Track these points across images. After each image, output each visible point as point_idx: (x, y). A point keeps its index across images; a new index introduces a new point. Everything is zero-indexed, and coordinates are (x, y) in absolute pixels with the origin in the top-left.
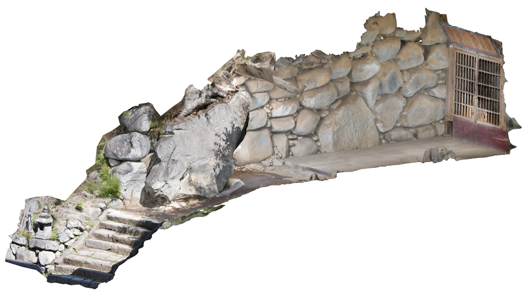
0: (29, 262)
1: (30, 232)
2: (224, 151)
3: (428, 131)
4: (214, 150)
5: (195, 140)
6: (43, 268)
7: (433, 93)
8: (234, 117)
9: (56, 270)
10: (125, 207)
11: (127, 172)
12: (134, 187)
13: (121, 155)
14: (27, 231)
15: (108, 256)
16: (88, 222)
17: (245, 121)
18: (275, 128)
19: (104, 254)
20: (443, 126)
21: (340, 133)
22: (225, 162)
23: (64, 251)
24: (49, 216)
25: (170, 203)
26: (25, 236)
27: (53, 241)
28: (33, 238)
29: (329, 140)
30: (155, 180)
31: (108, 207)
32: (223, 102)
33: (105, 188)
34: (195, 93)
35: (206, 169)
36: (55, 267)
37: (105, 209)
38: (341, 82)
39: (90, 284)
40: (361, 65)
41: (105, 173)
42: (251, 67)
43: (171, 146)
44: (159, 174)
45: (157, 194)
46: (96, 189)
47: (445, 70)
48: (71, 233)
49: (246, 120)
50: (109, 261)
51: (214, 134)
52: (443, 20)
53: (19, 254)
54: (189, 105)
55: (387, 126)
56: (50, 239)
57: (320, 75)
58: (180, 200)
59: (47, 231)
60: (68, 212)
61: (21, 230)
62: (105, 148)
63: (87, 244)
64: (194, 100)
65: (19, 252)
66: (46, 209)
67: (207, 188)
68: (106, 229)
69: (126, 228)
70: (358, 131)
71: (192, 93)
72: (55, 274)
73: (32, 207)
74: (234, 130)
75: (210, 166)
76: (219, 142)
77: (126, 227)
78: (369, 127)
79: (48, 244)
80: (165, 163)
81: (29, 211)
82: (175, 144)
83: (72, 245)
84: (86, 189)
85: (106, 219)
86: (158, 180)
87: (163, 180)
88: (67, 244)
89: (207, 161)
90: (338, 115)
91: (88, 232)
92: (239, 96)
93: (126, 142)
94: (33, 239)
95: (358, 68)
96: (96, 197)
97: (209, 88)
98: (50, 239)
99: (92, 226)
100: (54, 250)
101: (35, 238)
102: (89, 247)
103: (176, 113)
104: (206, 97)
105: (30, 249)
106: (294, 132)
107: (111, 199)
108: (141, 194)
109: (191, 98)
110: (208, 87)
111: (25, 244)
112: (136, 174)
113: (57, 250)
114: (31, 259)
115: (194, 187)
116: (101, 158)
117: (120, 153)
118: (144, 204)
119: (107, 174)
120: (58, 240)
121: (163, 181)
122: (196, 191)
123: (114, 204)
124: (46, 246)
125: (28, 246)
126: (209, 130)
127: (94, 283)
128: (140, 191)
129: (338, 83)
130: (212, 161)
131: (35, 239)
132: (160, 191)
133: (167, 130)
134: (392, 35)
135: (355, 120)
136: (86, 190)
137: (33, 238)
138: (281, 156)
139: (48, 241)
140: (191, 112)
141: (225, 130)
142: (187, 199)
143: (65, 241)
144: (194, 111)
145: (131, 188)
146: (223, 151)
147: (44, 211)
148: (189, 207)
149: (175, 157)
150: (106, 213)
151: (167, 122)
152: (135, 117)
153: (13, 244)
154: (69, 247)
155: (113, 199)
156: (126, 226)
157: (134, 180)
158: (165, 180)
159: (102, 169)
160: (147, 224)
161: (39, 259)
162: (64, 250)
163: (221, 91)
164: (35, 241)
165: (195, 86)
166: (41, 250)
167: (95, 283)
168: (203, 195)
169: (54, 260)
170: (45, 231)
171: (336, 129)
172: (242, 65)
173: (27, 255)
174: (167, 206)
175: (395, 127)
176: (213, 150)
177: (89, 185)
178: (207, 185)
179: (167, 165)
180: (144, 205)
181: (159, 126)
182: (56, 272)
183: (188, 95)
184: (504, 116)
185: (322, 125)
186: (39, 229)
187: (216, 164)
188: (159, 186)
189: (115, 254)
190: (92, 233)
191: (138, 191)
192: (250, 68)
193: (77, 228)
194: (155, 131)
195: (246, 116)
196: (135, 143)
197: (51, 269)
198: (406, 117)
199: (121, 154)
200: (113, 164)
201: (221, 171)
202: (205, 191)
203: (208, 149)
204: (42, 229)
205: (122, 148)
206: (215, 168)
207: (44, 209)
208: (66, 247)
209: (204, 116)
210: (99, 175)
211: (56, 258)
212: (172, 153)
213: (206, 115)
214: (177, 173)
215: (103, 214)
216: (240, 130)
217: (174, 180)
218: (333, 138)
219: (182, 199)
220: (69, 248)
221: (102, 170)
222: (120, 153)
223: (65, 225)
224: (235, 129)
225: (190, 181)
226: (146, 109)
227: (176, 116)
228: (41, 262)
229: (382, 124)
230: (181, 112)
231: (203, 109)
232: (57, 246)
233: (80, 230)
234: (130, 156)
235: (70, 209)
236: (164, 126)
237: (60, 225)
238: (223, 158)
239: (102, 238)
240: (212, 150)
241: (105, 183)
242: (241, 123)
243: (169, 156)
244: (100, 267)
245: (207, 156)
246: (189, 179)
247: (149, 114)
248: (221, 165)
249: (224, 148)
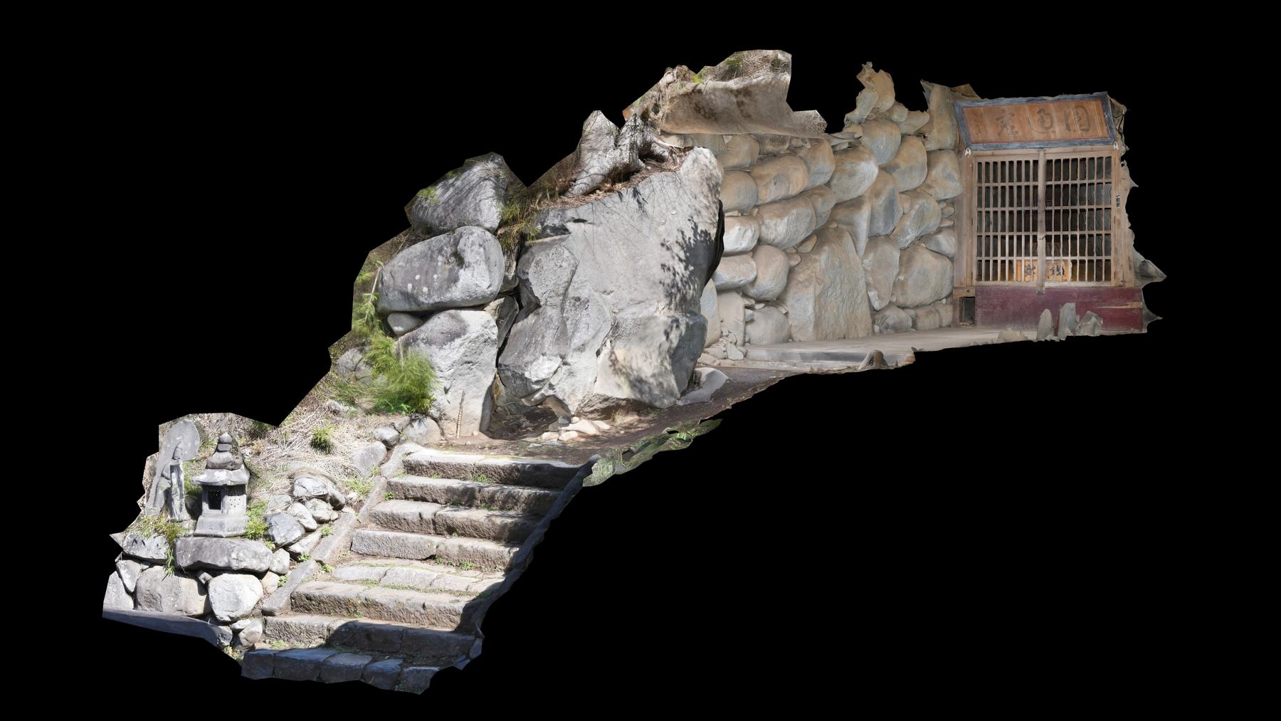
0: (179, 614)
1: (177, 518)
2: (684, 286)
4: (662, 281)
5: (618, 253)
6: (226, 629)
7: (938, 243)
8: (694, 206)
9: (269, 633)
10: (446, 440)
11: (452, 336)
12: (468, 385)
13: (429, 294)
14: (169, 517)
15: (437, 578)
16: (352, 480)
17: (717, 218)
18: (724, 277)
19: (419, 571)
20: (950, 308)
22: (688, 315)
23: (290, 572)
24: (237, 461)
25: (570, 422)
26: (163, 532)
27: (253, 541)
28: (189, 536)
30: (535, 356)
31: (403, 438)
32: (663, 170)
33: (386, 391)
34: (607, 134)
35: (648, 331)
36: (265, 623)
37: (395, 445)
38: (821, 195)
39: (399, 674)
40: (852, 163)
41: (383, 351)
42: (714, 95)
43: (564, 264)
44: (543, 337)
45: (537, 396)
46: (361, 394)
47: (952, 202)
48: (307, 515)
49: (719, 216)
50: (446, 591)
51: (658, 241)
52: (963, 95)
53: (144, 591)
54: (594, 163)
56: (243, 536)
58: (593, 416)
59: (232, 511)
60: (289, 456)
61: (150, 516)
62: (377, 285)
63: (357, 546)
64: (606, 150)
65: (144, 585)
66: (225, 440)
67: (655, 384)
68: (406, 498)
69: (473, 490)
72: (266, 646)
73: (180, 446)
74: (698, 238)
75: (658, 325)
76: (670, 263)
77: (472, 488)
79: (239, 551)
80: (554, 308)
81: (173, 458)
82: (575, 259)
83: (311, 551)
84: (333, 395)
86: (543, 355)
87: (556, 352)
88: (296, 548)
89: (652, 309)
91: (357, 509)
92: (697, 158)
93: (443, 256)
94: (190, 539)
95: (847, 168)
96: (367, 414)
97: (637, 124)
98: (243, 536)
99: (366, 493)
100: (257, 569)
101: (196, 535)
102: (364, 555)
103: (565, 182)
105: (180, 571)
106: (752, 292)
107: (407, 418)
109: (599, 145)
111: (163, 557)
112: (475, 342)
113: (268, 570)
114: (183, 603)
115: (625, 378)
116: (367, 312)
117: (425, 289)
118: (491, 432)
119: (386, 353)
120: (269, 538)
121: (556, 356)
122: (632, 388)
123: (418, 432)
124: (234, 555)
125: (173, 563)
126: (646, 231)
127: (412, 672)
128: (480, 396)
129: (817, 196)
130: (661, 312)
131: (196, 538)
132: (546, 387)
133: (549, 222)
136: (334, 396)
137: (189, 536)
139: (236, 541)
140: (600, 183)
141: (680, 235)
142: (608, 410)
143: (291, 540)
144: (607, 182)
145: (460, 386)
146: (684, 286)
147: (220, 449)
148: (622, 432)
149: (580, 291)
150: (400, 455)
151: (544, 206)
152: (457, 194)
153: (124, 561)
154: (302, 558)
155: (413, 417)
156: (470, 484)
157: (469, 363)
158: (563, 353)
159: (370, 343)
160: (538, 473)
161: (211, 600)
162: (290, 569)
164: (195, 544)
166: (216, 571)
167: (419, 671)
168: (647, 401)
169: (261, 600)
170: (225, 511)
171: (819, 288)
172: (686, 95)
173: (171, 590)
174: (562, 432)
176: (660, 282)
177: (340, 387)
178: (654, 376)
179: (562, 314)
180: (491, 435)
181: (523, 216)
182: (267, 641)
184: (1129, 258)
185: (794, 283)
186: (205, 506)
187: (670, 320)
188: (546, 371)
189: (453, 570)
190: (366, 514)
191: (477, 397)
192: (710, 99)
193: (323, 498)
194: (510, 234)
195: (717, 207)
196: (472, 251)
197: (252, 633)
198: (903, 284)
199: (429, 290)
200: (402, 327)
201: (682, 339)
202: (650, 389)
203: (648, 279)
204: (216, 504)
205: (430, 273)
206: (669, 330)
207: (220, 442)
208: (295, 557)
209: (631, 195)
210: (364, 360)
211: (266, 593)
212: (570, 282)
213: (636, 193)
214: (591, 332)
215: (392, 456)
216: (711, 238)
217: (583, 353)
218: (814, 309)
219: (596, 410)
220: (302, 561)
221: (373, 346)
222: (425, 289)
223: (286, 490)
224: (701, 236)
225: (614, 362)
226: (489, 170)
227: (563, 192)
228: (217, 612)
230: (575, 181)
231: (624, 181)
232: (268, 557)
233: (332, 504)
234: (456, 293)
235: (296, 448)
236: (535, 215)
237: (272, 491)
238: (683, 307)
239: (399, 527)
240: (658, 282)
241: (382, 379)
242: (709, 221)
243: (561, 291)
244: (418, 614)
245: (649, 297)
246: (611, 356)
247: (496, 184)
248: (683, 321)
249: (684, 279)
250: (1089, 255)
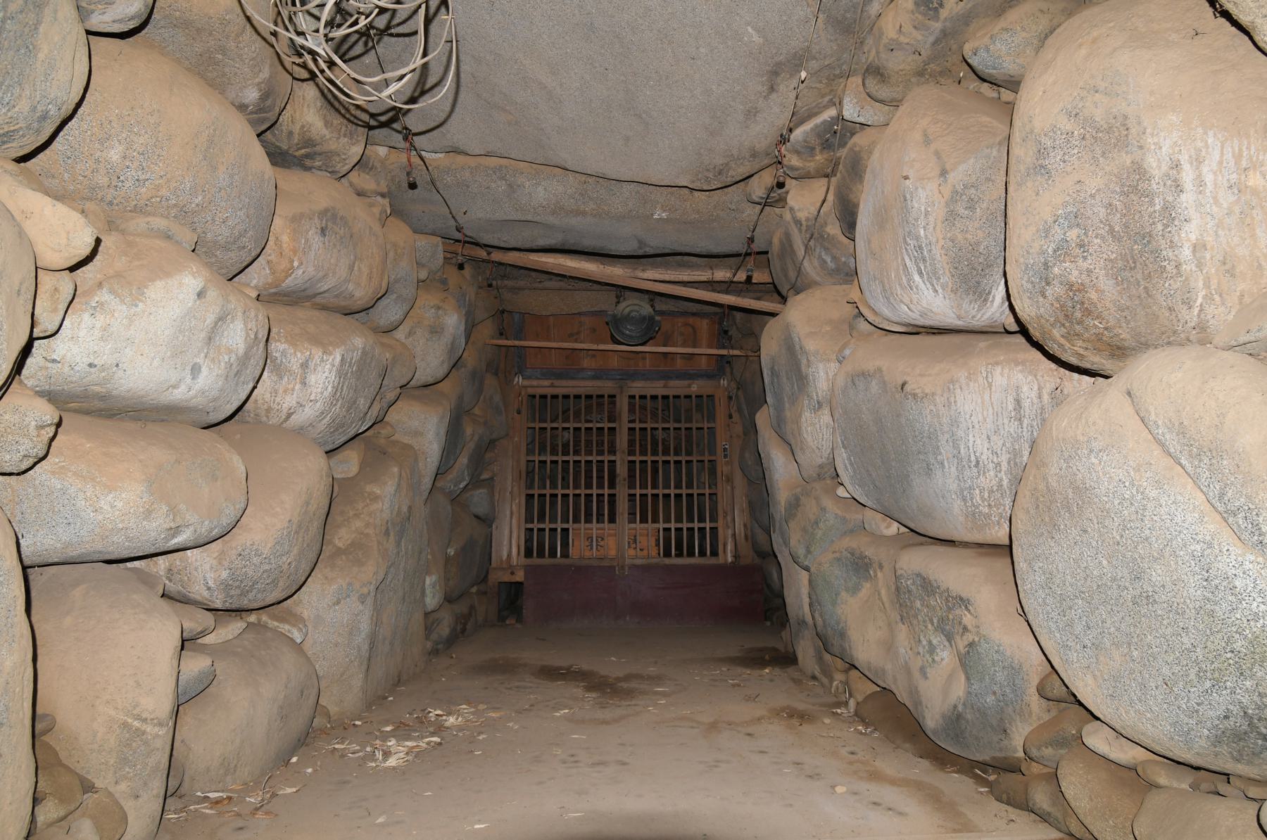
102: (302, 692)
250: (676, 522)
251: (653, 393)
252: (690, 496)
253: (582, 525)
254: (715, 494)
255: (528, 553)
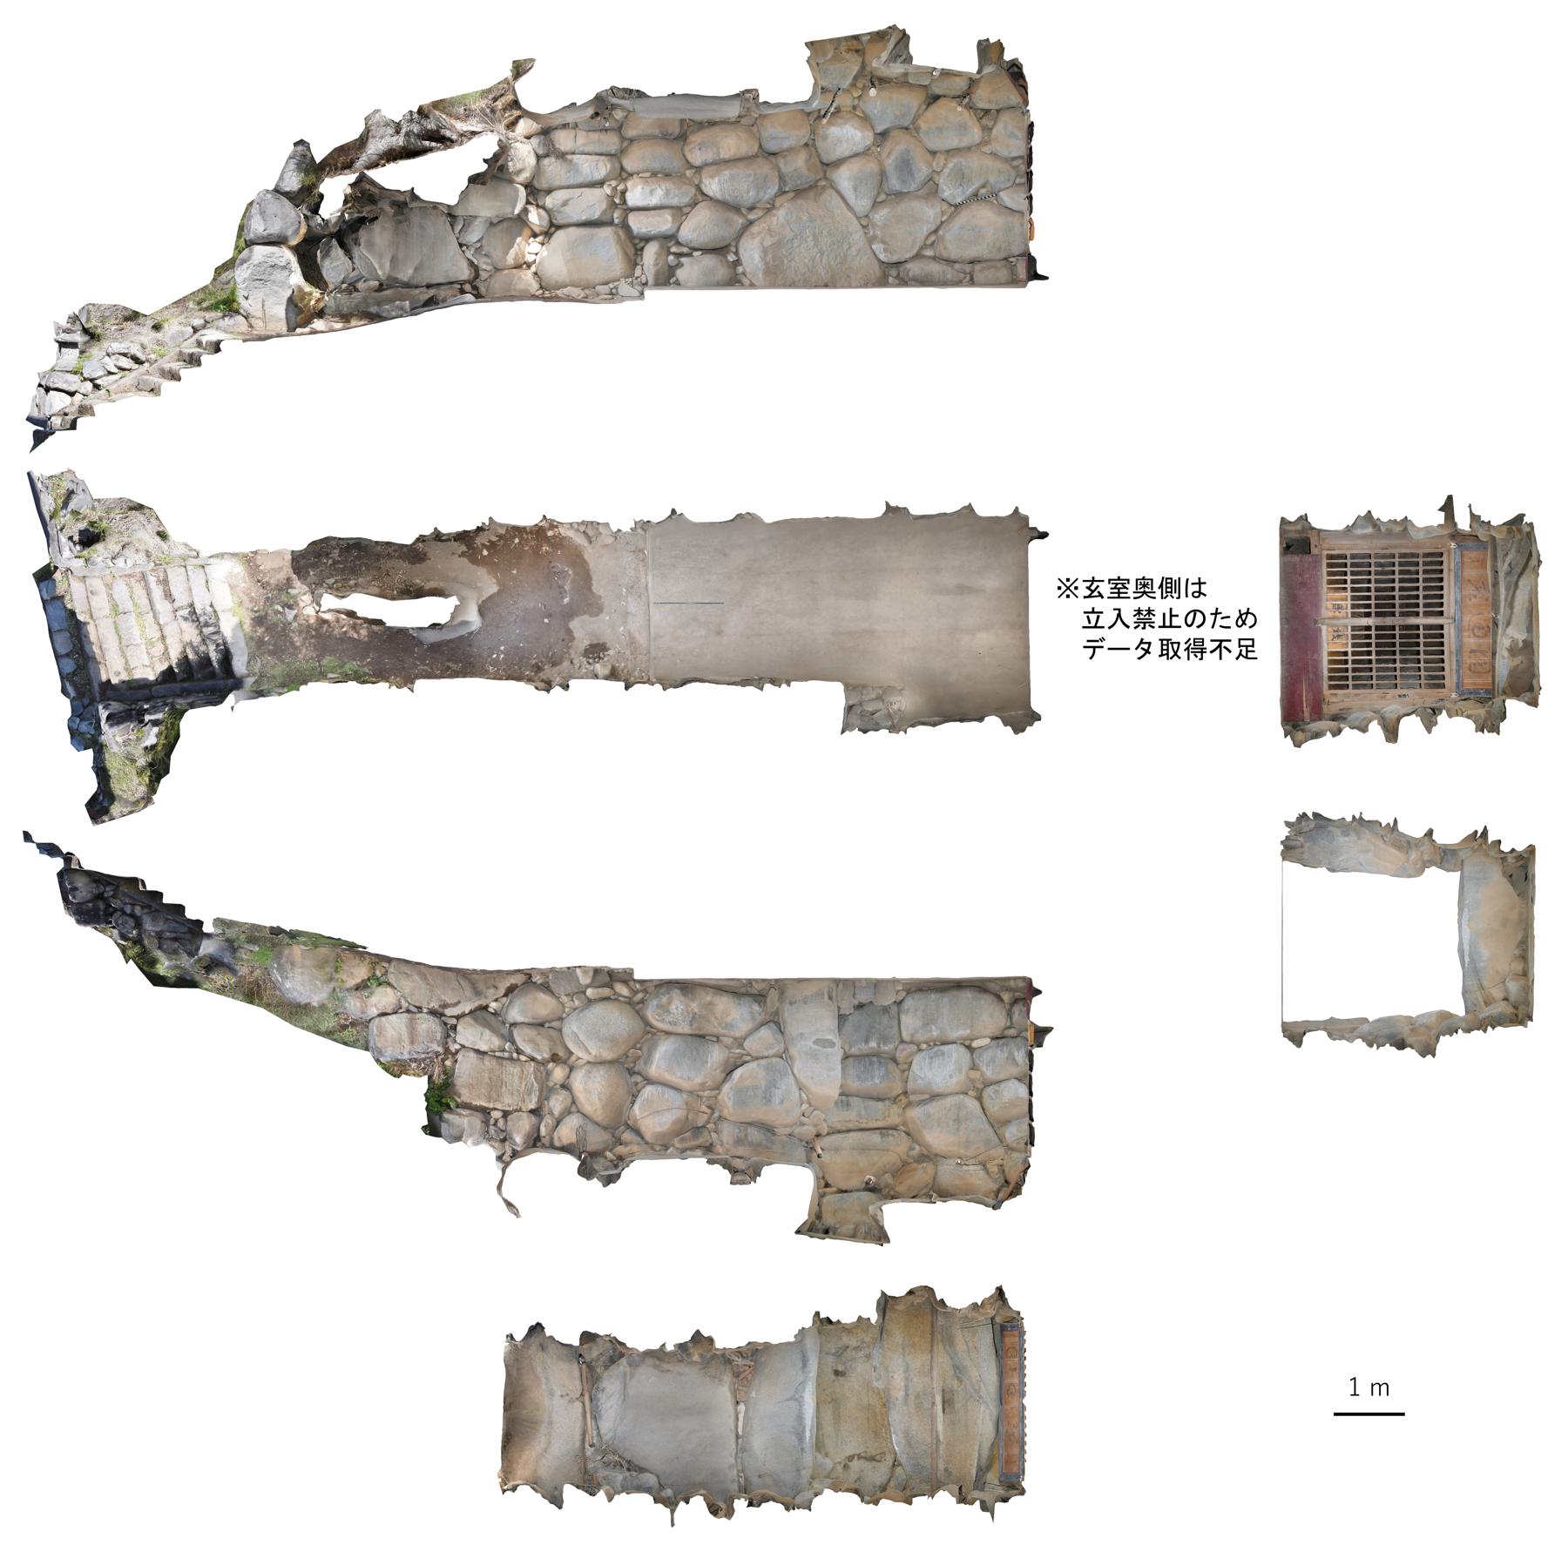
3: (993, 270)
21: (784, 252)
29: (756, 262)
55: (896, 251)
57: (726, 137)
64: (382, 137)
70: (826, 253)
71: (378, 125)
78: (853, 249)
85: (195, 345)
88: (98, 382)
90: (776, 218)
104: (407, 134)
107: (220, 314)
108: (287, 310)
110: (411, 115)
134: (902, 79)
135: (817, 231)
138: (644, 282)
143: (96, 376)
163: (449, 129)
165: (383, 113)
171: (768, 242)
175: (918, 256)
183: (372, 128)
185: (747, 233)
193: (125, 355)
208: (97, 387)
229: (882, 246)
251: (1445, 644)
252: (1371, 670)
253: (1349, 602)
254: (1396, 688)
255: (1330, 557)
